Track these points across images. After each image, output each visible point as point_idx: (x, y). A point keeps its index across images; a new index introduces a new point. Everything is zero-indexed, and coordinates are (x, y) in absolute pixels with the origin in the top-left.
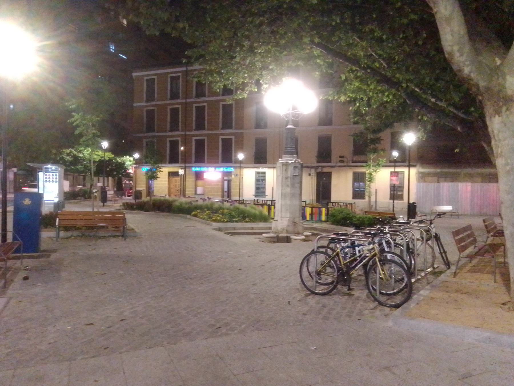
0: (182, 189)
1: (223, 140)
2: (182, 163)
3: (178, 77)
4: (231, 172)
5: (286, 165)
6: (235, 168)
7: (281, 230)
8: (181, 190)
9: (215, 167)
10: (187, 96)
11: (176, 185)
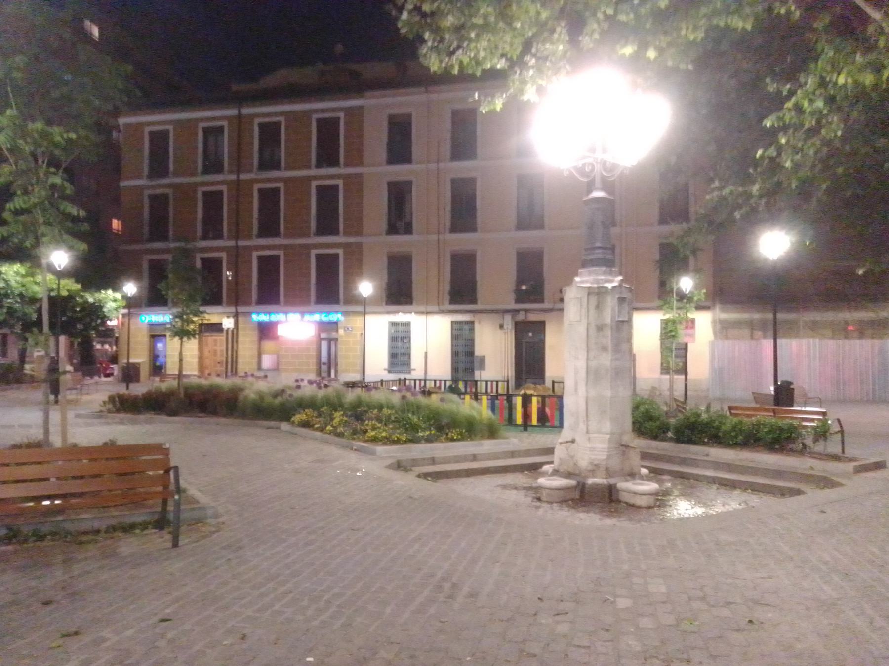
0: (230, 360)
1: (319, 257)
2: (229, 304)
3: (220, 130)
4: (336, 323)
5: (598, 293)
6: (345, 314)
7: (590, 467)
8: (227, 362)
9: (303, 314)
10: (239, 166)
11: (215, 351)
